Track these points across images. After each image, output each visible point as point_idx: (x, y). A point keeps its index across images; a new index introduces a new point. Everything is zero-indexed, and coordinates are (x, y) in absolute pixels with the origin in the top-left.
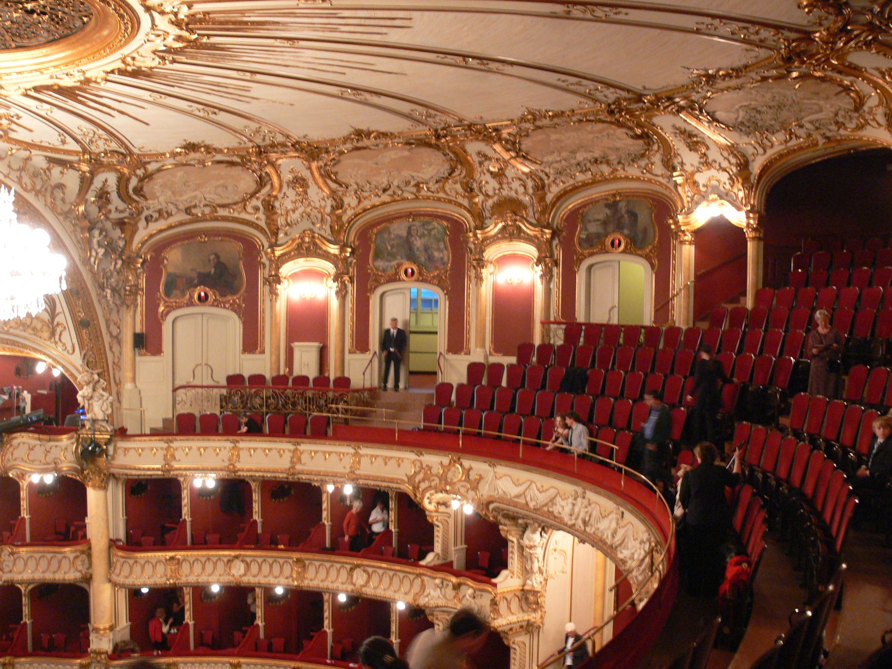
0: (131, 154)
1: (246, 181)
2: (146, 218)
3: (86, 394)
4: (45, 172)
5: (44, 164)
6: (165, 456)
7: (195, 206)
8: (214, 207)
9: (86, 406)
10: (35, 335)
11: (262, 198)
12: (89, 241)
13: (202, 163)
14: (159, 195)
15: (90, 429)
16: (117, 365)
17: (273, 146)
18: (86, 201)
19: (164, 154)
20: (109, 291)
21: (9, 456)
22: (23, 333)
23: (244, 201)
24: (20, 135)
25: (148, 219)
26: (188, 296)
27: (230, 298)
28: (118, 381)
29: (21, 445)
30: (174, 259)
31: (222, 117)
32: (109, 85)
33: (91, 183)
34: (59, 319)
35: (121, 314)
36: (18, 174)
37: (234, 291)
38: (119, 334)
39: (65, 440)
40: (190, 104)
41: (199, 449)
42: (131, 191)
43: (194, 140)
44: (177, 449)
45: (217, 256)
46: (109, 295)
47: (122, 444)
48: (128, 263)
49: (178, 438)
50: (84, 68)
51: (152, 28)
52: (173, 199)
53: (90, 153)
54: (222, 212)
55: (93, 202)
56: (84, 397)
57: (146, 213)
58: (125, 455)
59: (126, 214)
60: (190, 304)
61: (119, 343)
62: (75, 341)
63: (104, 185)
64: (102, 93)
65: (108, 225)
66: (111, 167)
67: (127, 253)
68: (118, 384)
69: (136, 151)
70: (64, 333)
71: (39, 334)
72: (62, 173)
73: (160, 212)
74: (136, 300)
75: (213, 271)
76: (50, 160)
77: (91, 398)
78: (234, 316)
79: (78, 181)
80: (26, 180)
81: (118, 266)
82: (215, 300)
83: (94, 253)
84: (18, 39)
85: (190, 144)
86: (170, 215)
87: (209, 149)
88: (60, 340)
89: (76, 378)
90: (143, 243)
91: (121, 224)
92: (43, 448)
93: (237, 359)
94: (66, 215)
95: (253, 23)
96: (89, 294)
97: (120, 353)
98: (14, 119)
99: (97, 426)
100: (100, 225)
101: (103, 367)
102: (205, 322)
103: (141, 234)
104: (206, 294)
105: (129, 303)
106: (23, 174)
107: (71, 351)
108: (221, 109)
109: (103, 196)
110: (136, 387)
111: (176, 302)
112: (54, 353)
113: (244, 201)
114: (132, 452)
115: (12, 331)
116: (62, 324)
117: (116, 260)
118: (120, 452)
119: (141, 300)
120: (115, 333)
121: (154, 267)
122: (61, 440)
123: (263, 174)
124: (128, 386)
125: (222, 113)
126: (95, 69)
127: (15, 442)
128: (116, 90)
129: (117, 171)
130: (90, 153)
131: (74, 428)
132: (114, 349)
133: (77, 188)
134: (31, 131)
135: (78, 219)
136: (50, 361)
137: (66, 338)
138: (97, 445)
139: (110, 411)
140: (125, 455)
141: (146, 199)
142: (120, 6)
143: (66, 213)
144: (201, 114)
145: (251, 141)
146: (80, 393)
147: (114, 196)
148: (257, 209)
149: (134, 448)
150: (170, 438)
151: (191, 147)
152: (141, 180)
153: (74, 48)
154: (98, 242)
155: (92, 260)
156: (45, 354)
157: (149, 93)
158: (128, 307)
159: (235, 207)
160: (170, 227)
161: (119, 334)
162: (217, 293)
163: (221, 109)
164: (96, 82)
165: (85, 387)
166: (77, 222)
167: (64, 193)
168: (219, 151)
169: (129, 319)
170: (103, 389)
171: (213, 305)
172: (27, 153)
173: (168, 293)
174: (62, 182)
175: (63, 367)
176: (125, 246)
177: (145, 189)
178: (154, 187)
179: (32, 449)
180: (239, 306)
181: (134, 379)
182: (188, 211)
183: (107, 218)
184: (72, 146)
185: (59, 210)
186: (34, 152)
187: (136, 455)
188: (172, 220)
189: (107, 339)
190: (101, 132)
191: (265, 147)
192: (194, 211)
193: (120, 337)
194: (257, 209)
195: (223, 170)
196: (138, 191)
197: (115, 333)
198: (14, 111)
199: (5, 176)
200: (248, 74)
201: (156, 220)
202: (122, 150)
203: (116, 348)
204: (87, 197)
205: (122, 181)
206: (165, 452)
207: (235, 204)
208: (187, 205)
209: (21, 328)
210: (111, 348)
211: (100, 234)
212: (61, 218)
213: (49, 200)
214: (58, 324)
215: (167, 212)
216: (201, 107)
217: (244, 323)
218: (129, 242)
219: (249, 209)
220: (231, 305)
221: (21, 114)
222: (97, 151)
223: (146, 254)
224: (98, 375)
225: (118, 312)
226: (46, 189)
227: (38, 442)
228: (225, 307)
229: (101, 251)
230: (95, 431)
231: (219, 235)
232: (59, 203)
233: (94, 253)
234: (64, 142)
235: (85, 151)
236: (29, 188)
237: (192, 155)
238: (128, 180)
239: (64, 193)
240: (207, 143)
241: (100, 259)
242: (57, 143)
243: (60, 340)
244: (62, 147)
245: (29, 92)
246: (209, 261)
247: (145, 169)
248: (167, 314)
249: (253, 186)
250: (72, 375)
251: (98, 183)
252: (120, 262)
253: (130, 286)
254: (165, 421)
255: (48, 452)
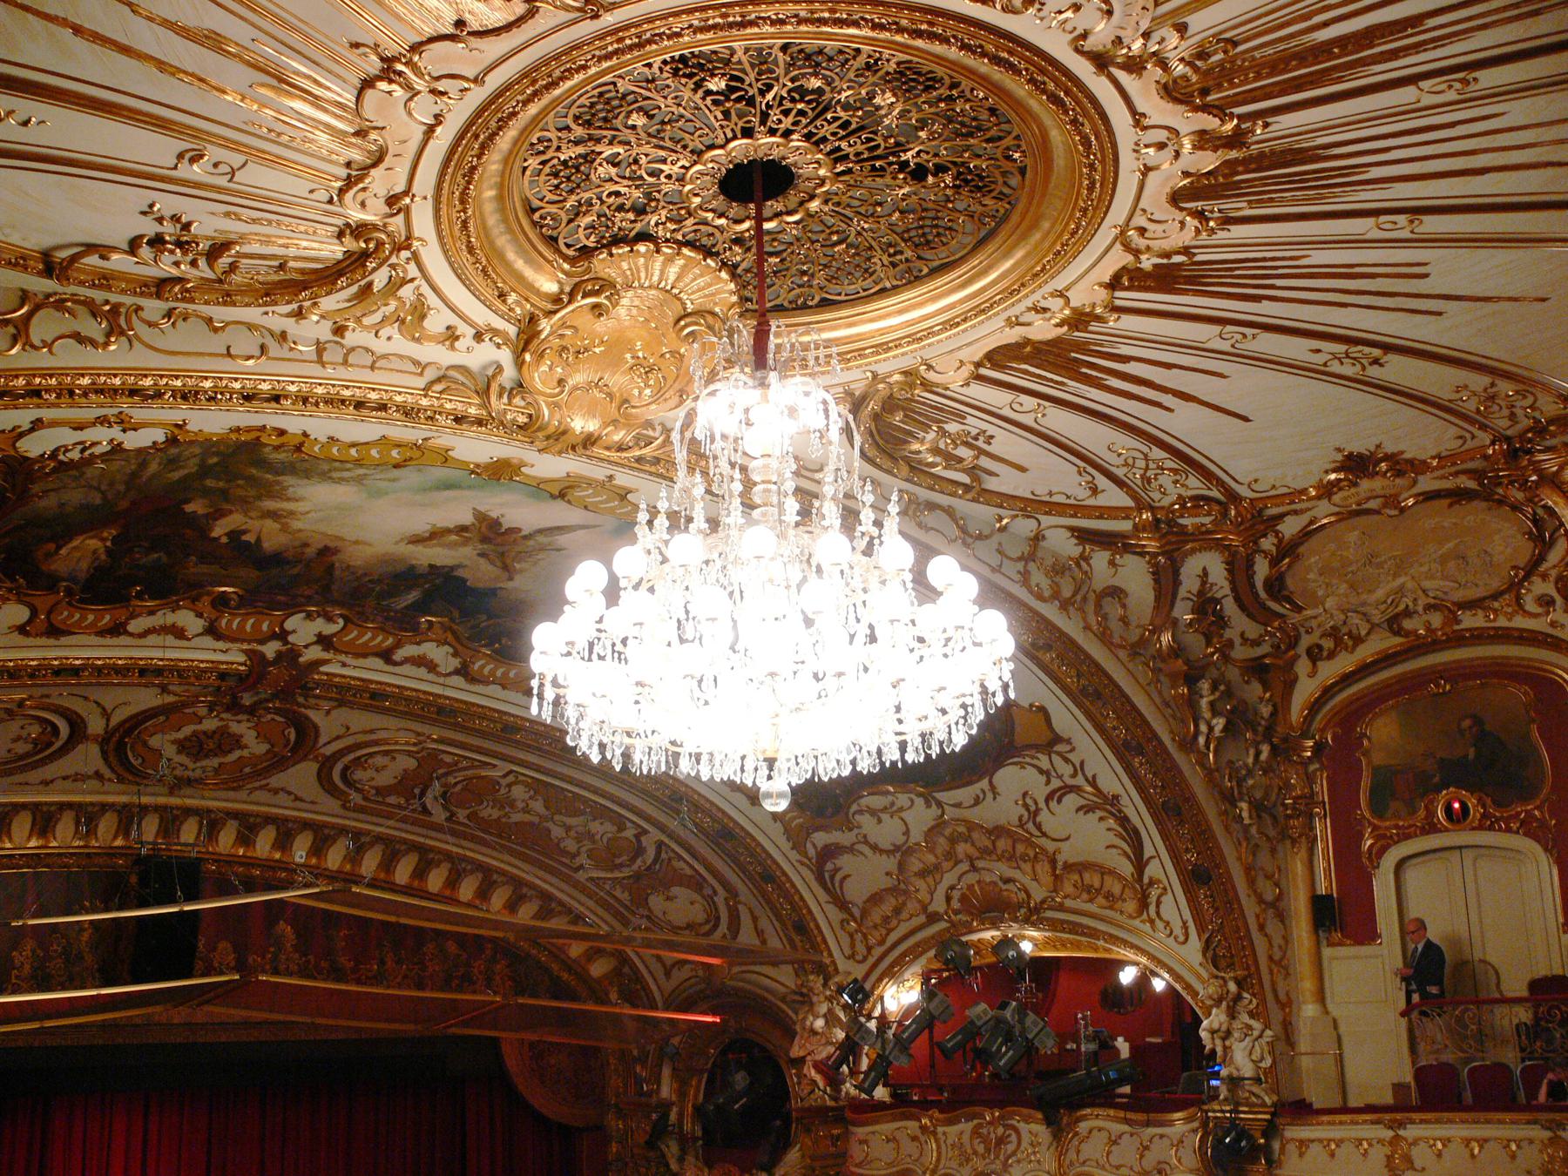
0: (1234, 497)
1: (1505, 540)
2: (1309, 652)
3: (1216, 1026)
4: (1078, 565)
5: (1071, 548)
6: (1389, 1158)
7: (1407, 613)
8: (1451, 611)
9: (1219, 1050)
10: (1111, 908)
11: (1554, 573)
12: (1191, 702)
13: (1392, 501)
14: (1325, 597)
15: (1226, 1099)
16: (1281, 964)
17: (1540, 430)
18: (1175, 623)
19: (1304, 491)
20: (1244, 805)
21: (1072, 1155)
22: (1092, 908)
23: (1514, 588)
24: (1005, 482)
25: (1315, 654)
26: (1422, 813)
27: (1521, 809)
28: (1282, 997)
29: (1095, 1132)
30: (1383, 735)
31: (1397, 370)
32: (1130, 323)
33: (1177, 583)
34: (1153, 870)
35: (1280, 855)
36: (1020, 566)
37: (1527, 794)
38: (1280, 897)
39: (1180, 1124)
40: (1316, 344)
41: (1467, 1142)
42: (1262, 594)
43: (1359, 446)
44: (1415, 1142)
45: (1477, 721)
46: (1245, 814)
47: (1295, 1132)
48: (1284, 750)
49: (1416, 1116)
50: (1060, 283)
51: (1137, 124)
52: (1354, 600)
53: (1152, 509)
54: (1471, 621)
55: (1190, 624)
56: (1213, 1032)
57: (1306, 641)
58: (1301, 1155)
59: (1265, 649)
60: (1431, 828)
61: (1282, 917)
62: (1187, 915)
63: (1204, 583)
64: (1125, 350)
65: (1233, 674)
66: (1204, 541)
67: (1281, 730)
68: (1286, 1004)
69: (1243, 491)
70: (1163, 899)
71: (1119, 905)
72: (1112, 563)
73: (1334, 633)
74: (1312, 828)
75: (1472, 753)
76: (1083, 536)
77: (1228, 1033)
78: (1537, 849)
79: (1148, 580)
80: (1039, 578)
81: (1264, 756)
82: (1484, 816)
83: (1203, 728)
84: (928, 254)
85: (1350, 456)
86: (1358, 640)
87: (1401, 466)
88: (1158, 913)
89: (1195, 994)
90: (1315, 707)
91: (1257, 669)
92: (1136, 1141)
93: (1554, 941)
94: (1136, 649)
95: (1343, 42)
96: (1201, 811)
97: (1286, 939)
98: (980, 443)
99: (1243, 1094)
100: (1214, 673)
101: (1248, 968)
102: (1468, 863)
103: (1306, 689)
104: (1464, 806)
105: (1295, 833)
106: (1032, 566)
107: (1182, 938)
108: (1387, 348)
109: (1205, 604)
110: (1327, 1013)
111: (1397, 827)
112: (1152, 945)
113: (1514, 588)
114: (1315, 1149)
115: (1068, 903)
116: (1159, 881)
117: (1256, 744)
118: (1292, 1148)
119: (1323, 829)
120: (1269, 897)
121: (1342, 755)
122: (1171, 1123)
123: (1540, 512)
124: (1310, 1010)
125: (1393, 359)
126: (1084, 278)
127: (1083, 1127)
128: (1136, 330)
129: (1219, 546)
130: (1152, 509)
131: (1196, 1098)
132: (1269, 929)
133: (1150, 596)
134: (1022, 469)
135: (1163, 660)
136: (1144, 960)
137: (1168, 909)
138: (1242, 1133)
139: (1267, 1063)
140: (1301, 1155)
141: (1299, 609)
142: (1042, 71)
143: (1133, 646)
144: (1348, 370)
145: (1483, 427)
146: (1205, 1023)
147: (1229, 607)
148: (1546, 602)
149: (1320, 1141)
150: (1399, 1116)
151: (1357, 465)
152: (1274, 562)
153: (1024, 237)
154: (1212, 704)
155: (1202, 740)
156: (1133, 946)
157: (1216, 329)
158: (1294, 842)
159: (1496, 605)
160: (1364, 670)
161: (1280, 897)
162: (1489, 801)
163: (1387, 348)
164: (1099, 318)
165: (1214, 1011)
166: (1161, 665)
167: (1124, 606)
168: (1418, 467)
169: (1299, 867)
170: (1252, 1015)
171: (1480, 828)
172: (1032, 524)
173: (1378, 808)
174: (1116, 582)
175: (1170, 971)
176: (1274, 714)
177: (1289, 582)
178: (1308, 574)
179: (1115, 1143)
180: (1543, 823)
181: (1321, 997)
182: (1394, 624)
183: (1226, 658)
184: (1113, 497)
185: (1117, 640)
186: (1047, 520)
187: (1325, 1157)
188: (1366, 652)
189: (1250, 907)
190: (1157, 453)
191: (1522, 436)
192: (1407, 624)
193: (1282, 905)
194: (1546, 602)
195: (1441, 517)
196: (1276, 586)
197: (1269, 897)
198: (974, 423)
199: (993, 570)
200: (1402, 219)
201: (1331, 655)
202: (1215, 493)
203: (1273, 927)
204: (1176, 613)
205: (1239, 569)
206: (1387, 1150)
207: (1495, 596)
208: (1391, 612)
209: (1085, 896)
210: (1262, 927)
211: (1214, 688)
212: (1122, 654)
213: (1092, 619)
214: (1151, 883)
215: (1350, 634)
216: (1340, 348)
217: (1560, 862)
218: (1280, 707)
219: (1531, 606)
220: (1523, 823)
221: (991, 430)
222: (1166, 502)
223: (1323, 731)
224: (1239, 983)
225: (1273, 851)
226: (1085, 599)
227: (1126, 1128)
228: (1509, 830)
229: (1219, 723)
230: (1237, 1104)
231: (1476, 676)
232: (1115, 625)
233: (1203, 728)
234: (1095, 491)
235: (1141, 506)
236: (1047, 594)
237: (1365, 485)
238: (1250, 564)
239: (1124, 606)
240: (1390, 448)
241: (1218, 739)
242: (1082, 494)
243: (1158, 913)
244: (1091, 502)
245: (983, 371)
246: (1461, 732)
247: (1277, 533)
248: (1382, 851)
249: (1524, 550)
250: (1188, 987)
251: (1189, 582)
252: (1265, 750)
253: (1295, 799)
254: (1398, 1088)
255: (1146, 1148)
